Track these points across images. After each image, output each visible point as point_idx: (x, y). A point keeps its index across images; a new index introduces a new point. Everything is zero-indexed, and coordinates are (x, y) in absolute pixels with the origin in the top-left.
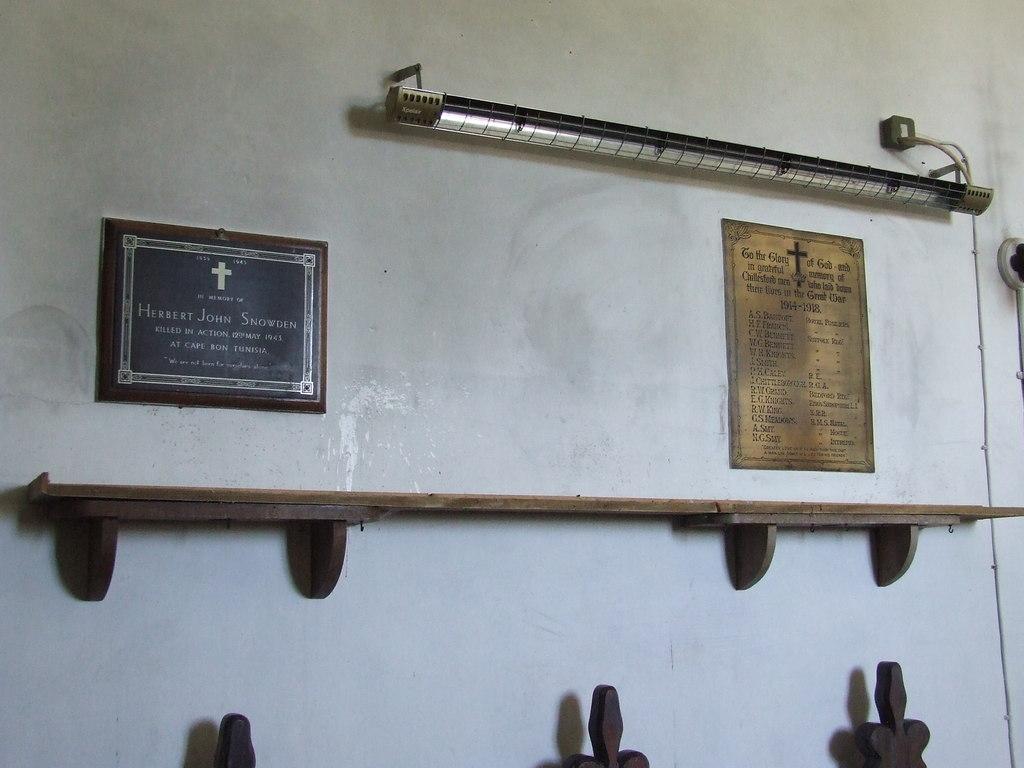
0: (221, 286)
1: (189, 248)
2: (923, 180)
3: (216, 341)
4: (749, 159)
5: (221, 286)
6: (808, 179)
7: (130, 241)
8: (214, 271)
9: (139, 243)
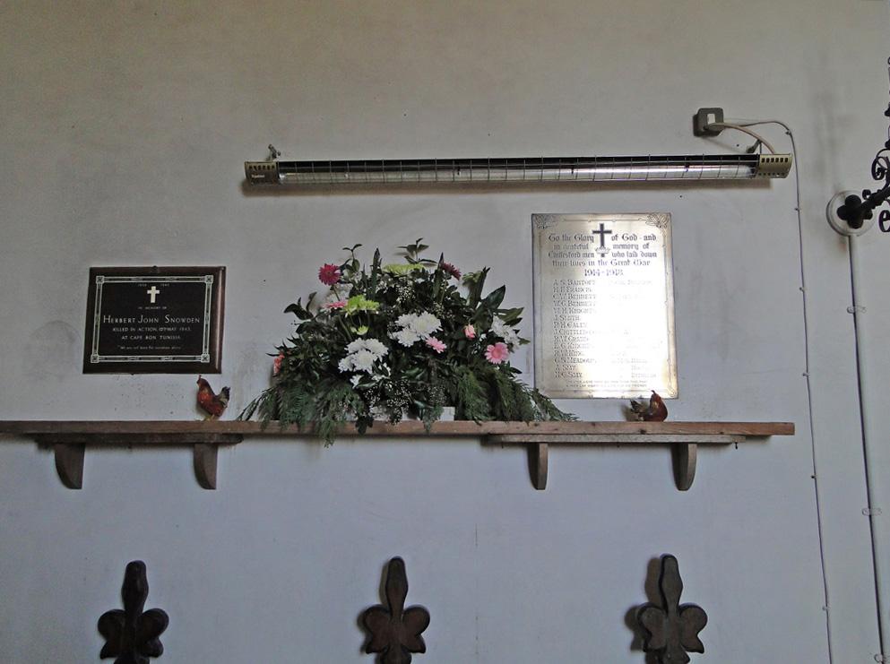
0: (153, 300)
1: (134, 280)
2: (743, 157)
3: (149, 333)
4: (706, 164)
5: (153, 300)
6: (700, 170)
7: (100, 280)
8: (149, 292)
9: (105, 280)
